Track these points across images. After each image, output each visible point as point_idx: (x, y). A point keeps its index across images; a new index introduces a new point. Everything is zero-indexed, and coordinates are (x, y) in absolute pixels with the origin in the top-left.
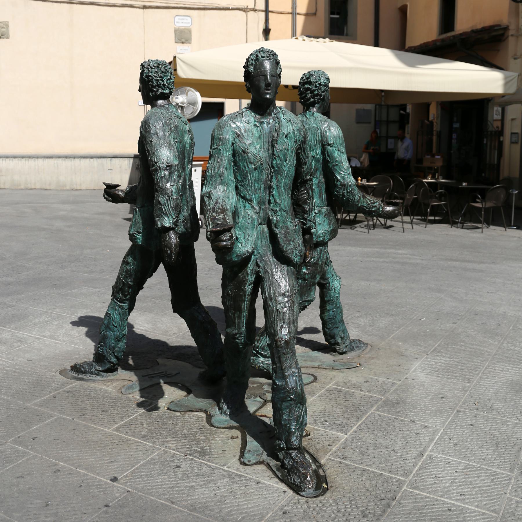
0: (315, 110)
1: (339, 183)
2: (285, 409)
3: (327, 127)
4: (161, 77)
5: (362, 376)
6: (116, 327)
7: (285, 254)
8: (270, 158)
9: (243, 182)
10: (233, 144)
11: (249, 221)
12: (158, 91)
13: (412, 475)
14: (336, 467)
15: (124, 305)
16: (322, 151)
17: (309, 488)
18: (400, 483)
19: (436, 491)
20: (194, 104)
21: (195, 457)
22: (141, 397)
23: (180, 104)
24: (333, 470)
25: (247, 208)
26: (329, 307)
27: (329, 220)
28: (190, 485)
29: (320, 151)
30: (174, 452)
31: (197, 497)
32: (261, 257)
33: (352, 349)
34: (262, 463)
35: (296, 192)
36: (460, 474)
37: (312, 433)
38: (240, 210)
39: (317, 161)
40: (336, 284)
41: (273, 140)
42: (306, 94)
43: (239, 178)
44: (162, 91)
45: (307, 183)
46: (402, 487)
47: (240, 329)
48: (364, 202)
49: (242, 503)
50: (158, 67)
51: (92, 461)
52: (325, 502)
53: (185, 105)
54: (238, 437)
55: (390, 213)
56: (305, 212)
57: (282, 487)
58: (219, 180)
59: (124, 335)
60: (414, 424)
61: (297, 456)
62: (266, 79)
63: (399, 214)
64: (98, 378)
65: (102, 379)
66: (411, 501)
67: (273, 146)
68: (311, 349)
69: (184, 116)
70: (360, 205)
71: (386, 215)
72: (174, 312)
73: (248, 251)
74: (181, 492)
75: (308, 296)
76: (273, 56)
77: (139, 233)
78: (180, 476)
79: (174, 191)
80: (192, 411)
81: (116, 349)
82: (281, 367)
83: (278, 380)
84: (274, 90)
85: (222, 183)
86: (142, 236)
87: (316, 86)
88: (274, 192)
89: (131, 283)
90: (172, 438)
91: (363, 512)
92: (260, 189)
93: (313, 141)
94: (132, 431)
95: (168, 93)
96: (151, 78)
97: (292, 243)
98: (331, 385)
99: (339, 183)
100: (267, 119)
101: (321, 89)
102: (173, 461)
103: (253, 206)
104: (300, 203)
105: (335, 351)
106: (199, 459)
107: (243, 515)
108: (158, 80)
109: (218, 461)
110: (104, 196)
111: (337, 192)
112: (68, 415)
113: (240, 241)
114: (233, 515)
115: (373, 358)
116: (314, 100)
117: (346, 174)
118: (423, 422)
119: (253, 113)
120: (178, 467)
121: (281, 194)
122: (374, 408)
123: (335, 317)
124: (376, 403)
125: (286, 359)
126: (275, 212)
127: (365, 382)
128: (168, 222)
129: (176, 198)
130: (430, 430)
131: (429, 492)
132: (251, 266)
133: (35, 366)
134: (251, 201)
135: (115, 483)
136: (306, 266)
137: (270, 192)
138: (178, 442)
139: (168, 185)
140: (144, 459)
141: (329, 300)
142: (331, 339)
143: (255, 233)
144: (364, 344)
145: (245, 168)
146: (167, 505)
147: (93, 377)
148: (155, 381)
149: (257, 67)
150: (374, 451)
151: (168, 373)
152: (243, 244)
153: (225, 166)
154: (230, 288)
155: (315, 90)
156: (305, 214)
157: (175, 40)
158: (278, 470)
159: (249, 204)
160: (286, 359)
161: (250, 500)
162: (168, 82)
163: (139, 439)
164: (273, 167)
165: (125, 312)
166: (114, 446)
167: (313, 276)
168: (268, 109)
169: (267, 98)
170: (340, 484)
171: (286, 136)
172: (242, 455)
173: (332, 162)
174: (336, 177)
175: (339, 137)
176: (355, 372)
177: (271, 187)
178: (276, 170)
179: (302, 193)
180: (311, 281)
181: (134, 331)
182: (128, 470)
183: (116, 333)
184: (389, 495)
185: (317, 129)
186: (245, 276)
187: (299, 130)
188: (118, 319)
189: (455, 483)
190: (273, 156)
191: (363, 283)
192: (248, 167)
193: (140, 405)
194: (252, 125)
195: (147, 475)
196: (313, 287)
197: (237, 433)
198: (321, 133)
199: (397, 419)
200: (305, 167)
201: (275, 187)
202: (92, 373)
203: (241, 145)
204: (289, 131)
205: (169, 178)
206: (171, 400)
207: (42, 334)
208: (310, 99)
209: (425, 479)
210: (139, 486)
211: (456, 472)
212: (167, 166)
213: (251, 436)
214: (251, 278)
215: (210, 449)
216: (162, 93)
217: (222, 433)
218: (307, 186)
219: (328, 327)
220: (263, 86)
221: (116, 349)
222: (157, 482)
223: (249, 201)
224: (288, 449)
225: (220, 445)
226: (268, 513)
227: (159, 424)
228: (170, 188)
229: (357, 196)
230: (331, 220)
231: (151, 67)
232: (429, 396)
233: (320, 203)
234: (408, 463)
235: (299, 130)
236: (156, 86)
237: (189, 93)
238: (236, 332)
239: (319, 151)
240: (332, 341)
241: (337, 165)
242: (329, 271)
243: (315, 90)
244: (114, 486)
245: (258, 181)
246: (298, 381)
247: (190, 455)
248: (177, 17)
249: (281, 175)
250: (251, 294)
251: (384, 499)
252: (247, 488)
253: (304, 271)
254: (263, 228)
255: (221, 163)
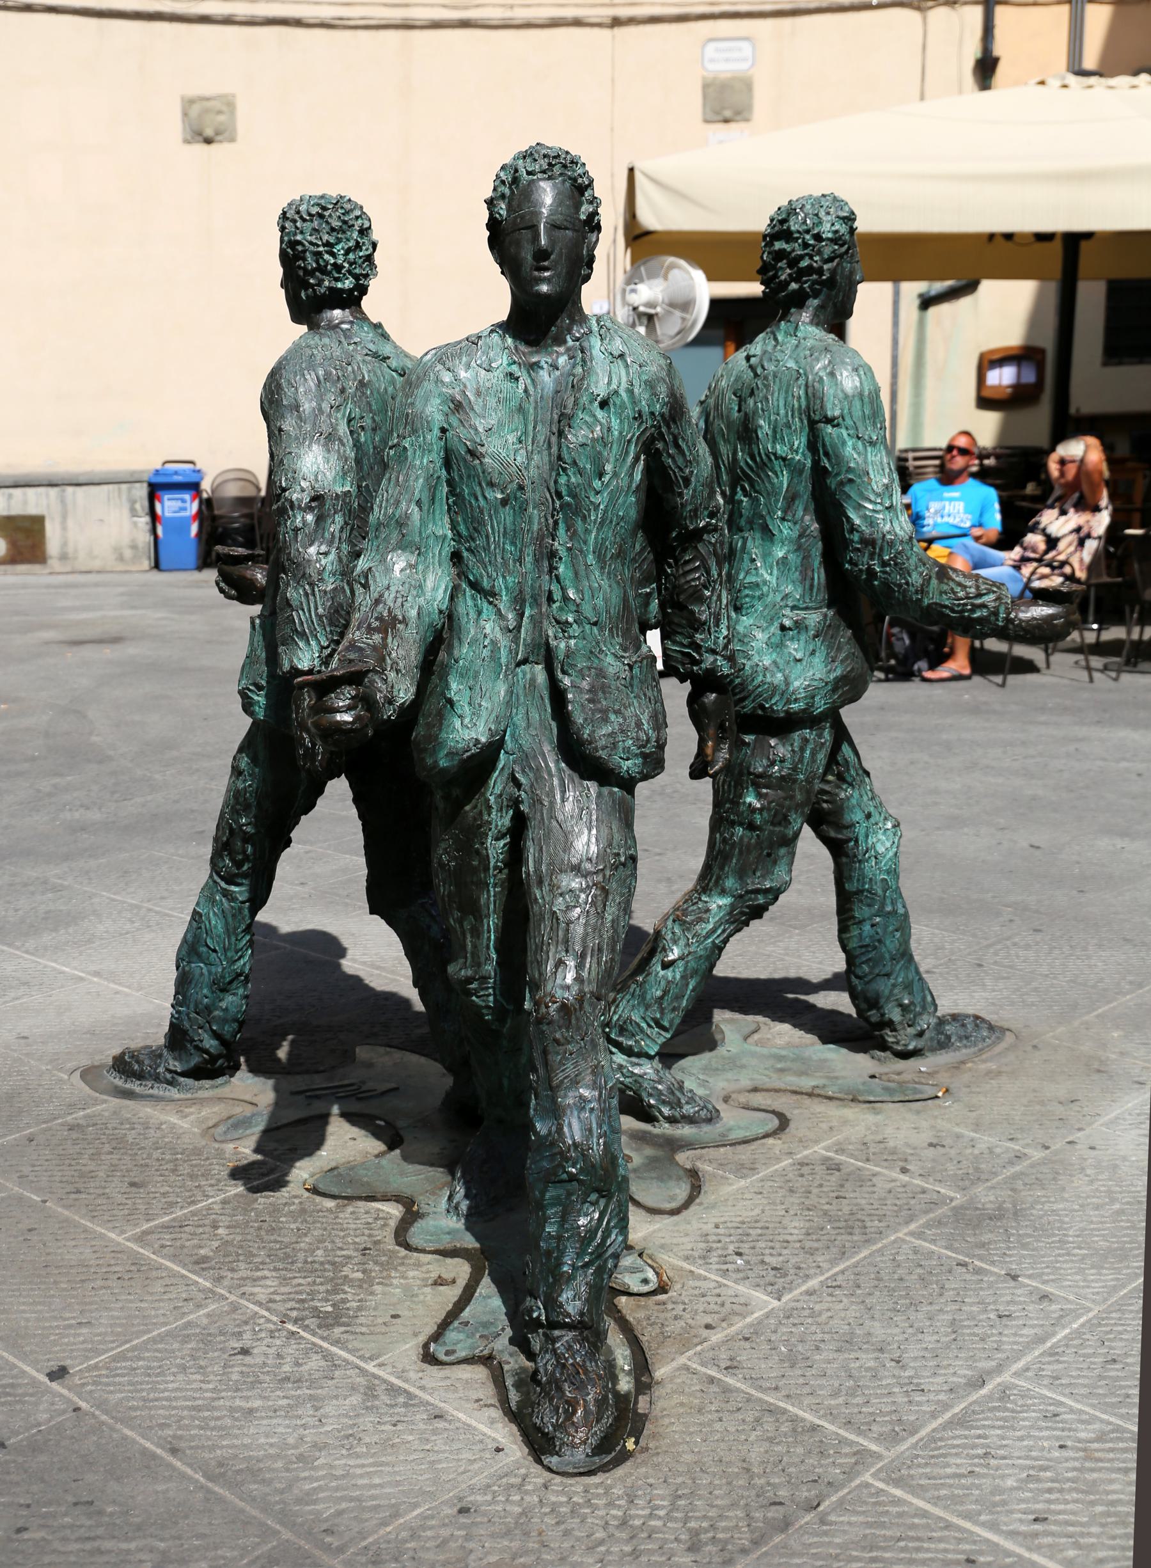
0: (806, 316)
1: (856, 537)
2: (553, 1205)
3: (825, 368)
4: (327, 244)
5: (933, 1127)
6: (214, 951)
7: (588, 749)
8: (551, 469)
9: (474, 540)
10: (443, 430)
11: (486, 653)
12: (320, 284)
13: (913, 1440)
14: (691, 1394)
15: (236, 889)
16: (809, 441)
17: (573, 1446)
18: (862, 1457)
19: (956, 1500)
20: (686, 306)
21: (306, 1328)
22: (257, 1150)
23: (642, 309)
24: (677, 1399)
25: (484, 616)
26: (860, 911)
27: (830, 647)
28: (249, 1405)
29: (804, 440)
30: (256, 1309)
31: (247, 1441)
32: (525, 758)
33: (943, 1044)
34: (486, 1360)
35: (670, 566)
36: (1071, 1454)
37: (678, 1286)
38: (464, 620)
39: (796, 470)
40: (882, 843)
41: (562, 414)
42: (777, 271)
43: (462, 528)
44: (333, 284)
45: (701, 540)
46: (858, 1474)
47: (479, 965)
48: (941, 593)
49: (359, 1471)
50: (321, 216)
51: (27, 1320)
52: (601, 1491)
53: (659, 309)
54: (454, 1281)
55: (1038, 626)
56: (697, 625)
57: (505, 1434)
58: (395, 536)
59: (240, 975)
60: (1012, 1284)
61: (569, 1348)
62: (536, 237)
63: (1070, 626)
64: (174, 1093)
65: (182, 1096)
66: (861, 1519)
67: (561, 434)
68: (820, 1038)
69: (657, 342)
70: (926, 602)
71: (1023, 629)
72: (372, 911)
73: (477, 741)
74: (212, 1424)
75: (763, 876)
76: (565, 166)
77: (259, 688)
78: (235, 1377)
79: (329, 568)
80: (371, 1198)
81: (217, 1013)
82: (550, 1080)
83: (542, 1119)
84: (562, 269)
85: (403, 545)
86: (266, 696)
87: (805, 245)
88: (562, 569)
89: (249, 829)
90: (275, 1269)
91: (695, 1533)
92: (520, 560)
93: (782, 412)
94: (178, 1244)
95: (351, 291)
96: (300, 248)
97: (612, 717)
98: (820, 1150)
99: (856, 537)
100: (550, 354)
101: (819, 253)
102: (240, 1334)
103: (499, 610)
104: (682, 597)
105: (884, 1047)
106: (314, 1335)
107: (344, 1505)
108: (319, 254)
109: (360, 1346)
110: (217, 584)
111: (851, 562)
112: (36, 1191)
113: (459, 712)
114: (315, 1502)
115: (999, 1073)
116: (801, 288)
117: (879, 507)
118: (1044, 1282)
119: (509, 341)
120: (245, 1352)
121: (582, 573)
122: (912, 1226)
123: (880, 941)
124: (926, 1212)
125: (564, 1058)
126: (564, 625)
127: (931, 1145)
128: (308, 656)
129: (335, 589)
130: (1054, 1307)
131: (936, 1501)
132: (497, 784)
133: (27, 1055)
134: (494, 595)
135: (55, 1386)
136: (757, 786)
137: (552, 569)
138: (284, 1281)
139: (312, 550)
140: (165, 1324)
141: (860, 892)
142: (870, 1009)
143: (502, 689)
144: (991, 1028)
145: (477, 499)
146: (154, 1456)
147: (159, 1090)
148: (317, 1107)
149: (514, 203)
150: (836, 1355)
151: (364, 1088)
152: (467, 721)
153: (417, 496)
154: (443, 845)
155: (801, 257)
156: (696, 630)
157: (704, 113)
158: (518, 1385)
159: (491, 603)
160: (564, 1058)
161: (387, 1464)
162: (351, 256)
163: (184, 1266)
164: (559, 495)
165: (240, 909)
166: (109, 1283)
167: (779, 817)
168: (553, 323)
169: (539, 295)
170: (675, 1444)
171: (604, 404)
172: (436, 1337)
173: (838, 474)
174: (848, 518)
175: (861, 395)
176: (918, 1112)
177: (553, 554)
178: (569, 504)
179: (688, 568)
180: (772, 833)
181: (339, 966)
182: (106, 1351)
183: (213, 969)
184: (804, 1493)
185: (795, 374)
186: (481, 813)
187: (650, 385)
188: (220, 929)
189: (1039, 1480)
190: (559, 464)
191: (1104, 843)
192: (485, 498)
193: (239, 1173)
194: (498, 374)
195: (149, 1368)
196: (783, 851)
197: (461, 1270)
198: (807, 386)
199: (965, 1265)
200: (688, 494)
201: (563, 553)
202: (157, 1078)
203: (463, 433)
204: (614, 386)
205: (316, 531)
206: (333, 1164)
207: (93, 968)
208: (787, 283)
209: (944, 1456)
210: (111, 1397)
211: (1061, 1447)
212: (313, 499)
213: (494, 1280)
214: (502, 820)
215: (359, 1309)
216: (331, 289)
217: (418, 1265)
218: (700, 546)
219: (859, 972)
220: (529, 258)
221: (217, 1013)
222: (165, 1390)
223: (490, 595)
224: (553, 1325)
225: (395, 1300)
226: (416, 1506)
227: (260, 1228)
228: (317, 561)
229: (915, 575)
230: (839, 649)
231: (301, 218)
232: (1113, 1201)
233: (803, 596)
234: (919, 1404)
235: (650, 385)
236: (314, 270)
237: (675, 274)
238: (470, 973)
239: (800, 442)
240: (874, 1016)
241: (851, 481)
242: (854, 801)
243: (801, 257)
244: (48, 1391)
245: (514, 536)
246: (594, 1126)
247: (296, 1321)
248: (711, 47)
249: (584, 518)
250: (507, 864)
251: (781, 1504)
252: (399, 1427)
253: (748, 800)
254: (533, 674)
255: (405, 488)
